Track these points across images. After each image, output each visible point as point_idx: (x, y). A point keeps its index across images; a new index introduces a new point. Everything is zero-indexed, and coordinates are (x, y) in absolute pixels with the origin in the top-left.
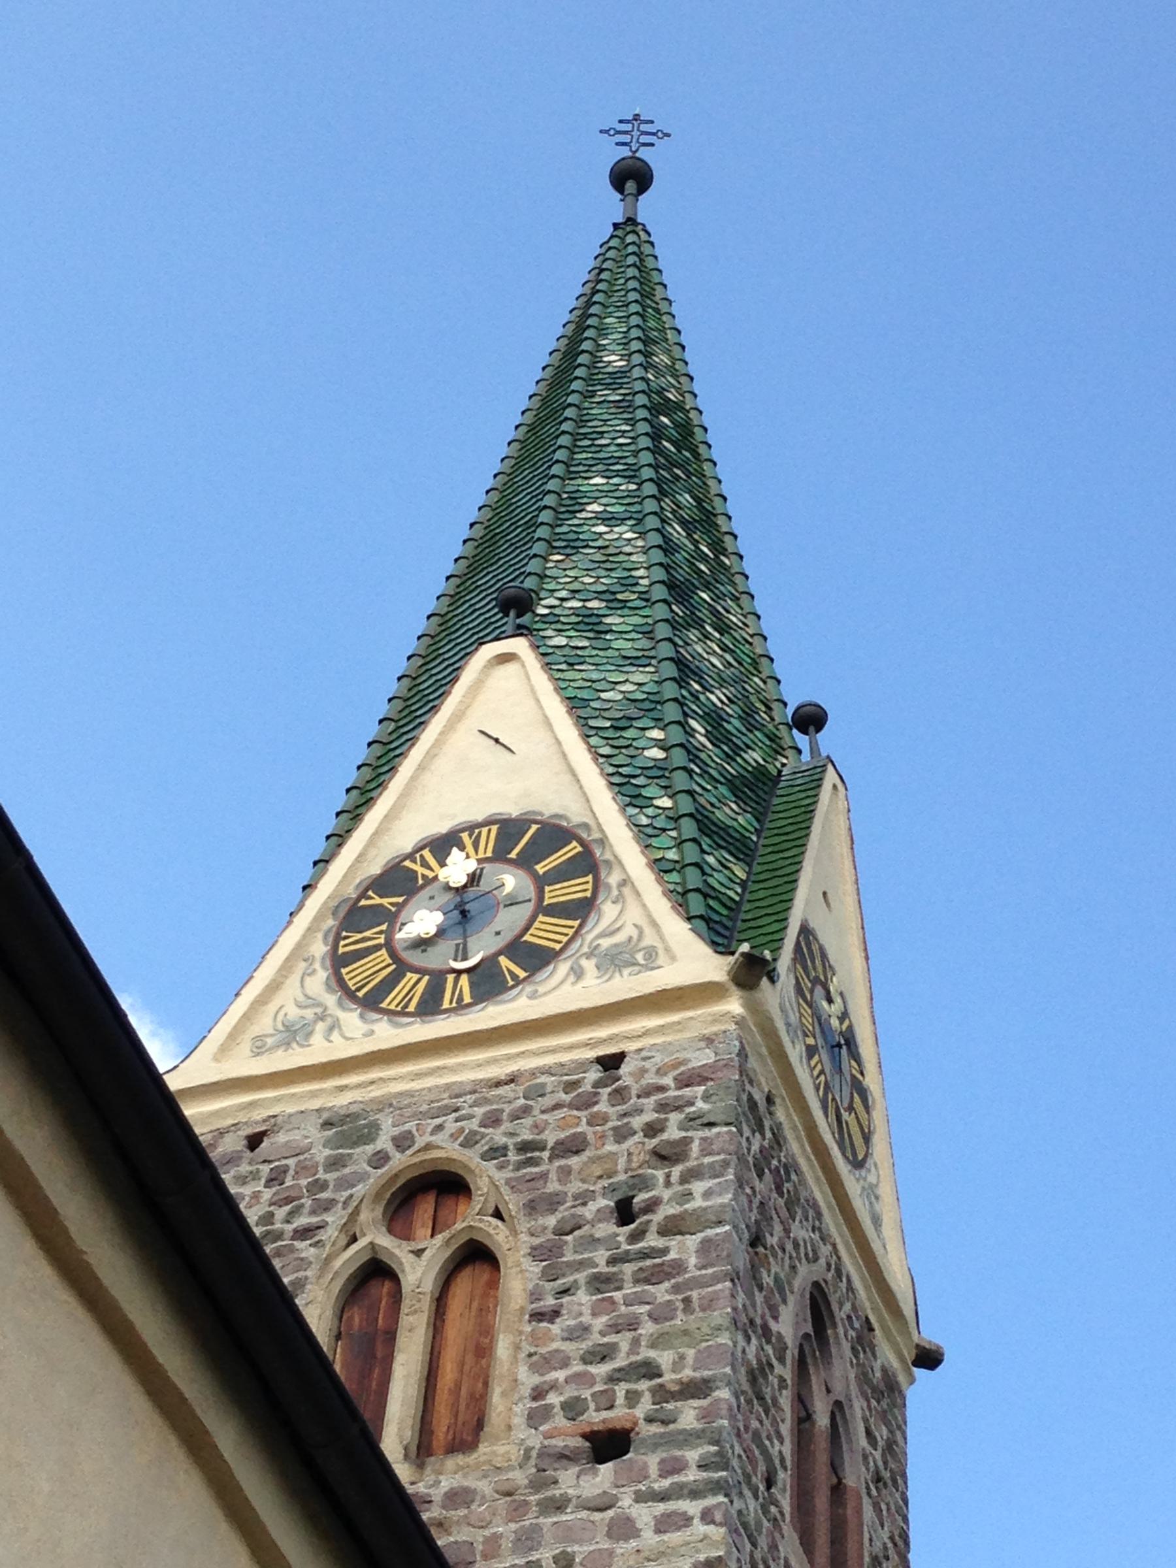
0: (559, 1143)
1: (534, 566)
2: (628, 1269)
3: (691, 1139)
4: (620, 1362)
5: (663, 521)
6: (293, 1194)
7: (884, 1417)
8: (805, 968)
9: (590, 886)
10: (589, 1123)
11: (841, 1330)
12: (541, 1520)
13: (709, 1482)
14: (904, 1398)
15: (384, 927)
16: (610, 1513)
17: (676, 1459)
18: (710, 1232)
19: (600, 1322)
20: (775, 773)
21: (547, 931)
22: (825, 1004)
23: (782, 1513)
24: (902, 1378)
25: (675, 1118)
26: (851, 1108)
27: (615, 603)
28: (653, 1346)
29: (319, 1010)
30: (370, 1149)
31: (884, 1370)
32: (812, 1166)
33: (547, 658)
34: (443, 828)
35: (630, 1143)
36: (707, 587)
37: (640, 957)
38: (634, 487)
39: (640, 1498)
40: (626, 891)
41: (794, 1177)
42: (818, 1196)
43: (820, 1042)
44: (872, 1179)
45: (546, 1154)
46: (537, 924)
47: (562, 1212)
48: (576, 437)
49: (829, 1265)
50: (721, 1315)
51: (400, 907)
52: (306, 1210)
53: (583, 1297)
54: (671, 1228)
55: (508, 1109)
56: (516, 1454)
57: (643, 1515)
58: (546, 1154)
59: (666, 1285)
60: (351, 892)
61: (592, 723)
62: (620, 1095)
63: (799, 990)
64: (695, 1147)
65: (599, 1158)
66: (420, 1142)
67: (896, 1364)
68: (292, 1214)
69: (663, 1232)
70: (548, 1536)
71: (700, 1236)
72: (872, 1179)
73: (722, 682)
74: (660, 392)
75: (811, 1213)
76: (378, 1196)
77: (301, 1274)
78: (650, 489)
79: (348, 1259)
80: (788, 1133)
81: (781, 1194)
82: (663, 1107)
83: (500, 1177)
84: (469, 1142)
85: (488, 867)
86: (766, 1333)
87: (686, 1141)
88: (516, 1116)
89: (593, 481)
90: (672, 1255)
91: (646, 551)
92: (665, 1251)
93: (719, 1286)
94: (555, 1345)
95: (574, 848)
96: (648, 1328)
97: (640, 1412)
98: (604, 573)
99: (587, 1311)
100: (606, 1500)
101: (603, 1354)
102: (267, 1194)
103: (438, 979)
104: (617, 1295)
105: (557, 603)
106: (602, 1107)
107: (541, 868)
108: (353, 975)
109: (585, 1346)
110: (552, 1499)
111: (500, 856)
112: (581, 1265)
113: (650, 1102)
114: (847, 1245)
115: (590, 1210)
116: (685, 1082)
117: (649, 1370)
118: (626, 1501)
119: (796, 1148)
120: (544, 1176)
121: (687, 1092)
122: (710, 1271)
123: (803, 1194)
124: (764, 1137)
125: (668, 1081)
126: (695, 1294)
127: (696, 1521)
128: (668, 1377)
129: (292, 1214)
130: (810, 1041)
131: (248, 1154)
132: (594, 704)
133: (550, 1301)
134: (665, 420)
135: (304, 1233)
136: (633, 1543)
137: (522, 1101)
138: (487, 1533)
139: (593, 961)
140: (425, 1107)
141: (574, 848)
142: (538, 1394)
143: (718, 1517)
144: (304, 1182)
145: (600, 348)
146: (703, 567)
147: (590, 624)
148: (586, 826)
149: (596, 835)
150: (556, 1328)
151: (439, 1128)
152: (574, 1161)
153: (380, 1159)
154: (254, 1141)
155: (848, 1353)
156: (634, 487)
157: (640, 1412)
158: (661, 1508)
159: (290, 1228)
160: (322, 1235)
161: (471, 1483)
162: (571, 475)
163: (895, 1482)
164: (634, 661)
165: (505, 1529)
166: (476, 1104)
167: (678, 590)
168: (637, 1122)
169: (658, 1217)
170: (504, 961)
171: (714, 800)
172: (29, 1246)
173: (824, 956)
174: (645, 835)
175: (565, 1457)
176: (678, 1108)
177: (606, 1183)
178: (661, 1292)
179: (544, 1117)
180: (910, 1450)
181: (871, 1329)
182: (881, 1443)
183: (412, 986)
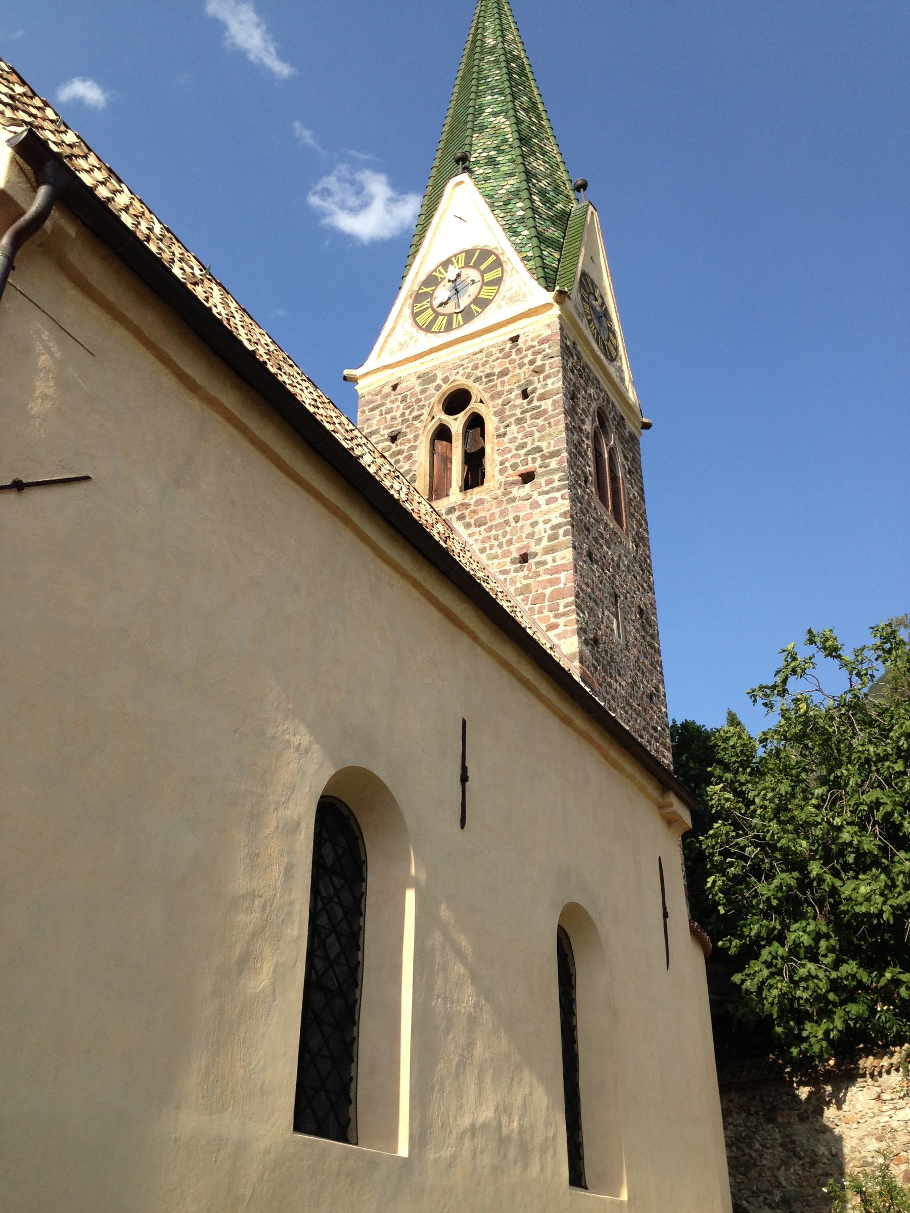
0: (500, 372)
1: (467, 141)
2: (528, 415)
3: (545, 364)
4: (529, 448)
5: (516, 111)
6: (411, 404)
7: (631, 450)
8: (585, 290)
9: (500, 272)
10: (510, 364)
11: (611, 422)
12: (508, 506)
13: (562, 485)
14: (638, 441)
15: (429, 300)
16: (530, 500)
17: (550, 479)
18: (555, 397)
19: (520, 435)
20: (569, 211)
21: (487, 293)
22: (594, 302)
23: (592, 492)
24: (637, 435)
25: (539, 357)
26: (609, 339)
27: (500, 151)
28: (539, 441)
29: (410, 335)
30: (434, 384)
31: (630, 433)
32: (594, 364)
33: (476, 181)
34: (445, 258)
35: (524, 368)
36: (536, 136)
37: (521, 298)
38: (503, 98)
39: (540, 494)
40: (514, 271)
41: (587, 370)
42: (597, 375)
43: (593, 316)
44: (619, 364)
45: (495, 377)
46: (483, 290)
47: (503, 397)
48: (478, 80)
49: (604, 400)
50: (562, 426)
51: (434, 291)
52: (416, 410)
53: (514, 428)
54: (542, 397)
55: (480, 362)
56: (497, 485)
57: (542, 500)
58: (495, 377)
59: (542, 419)
60: (416, 288)
61: (496, 204)
62: (519, 351)
63: (583, 298)
64: (547, 367)
65: (514, 376)
66: (451, 380)
67: (634, 430)
68: (411, 412)
69: (539, 399)
70: (510, 511)
71: (552, 399)
72: (619, 364)
73: (545, 177)
74: (510, 52)
75: (595, 382)
76: (439, 402)
77: (417, 433)
78: (509, 98)
79: (432, 426)
80: (583, 354)
81: (582, 378)
82: (535, 353)
83: (481, 388)
84: (468, 377)
85: (463, 270)
86: (581, 430)
87: (544, 365)
88: (483, 365)
89: (487, 99)
90: (543, 408)
91: (510, 126)
92: (540, 407)
93: (560, 416)
94: (505, 446)
95: (493, 258)
96: (537, 435)
97: (537, 464)
98: (494, 139)
99: (515, 432)
100: (529, 497)
101: (522, 446)
102: (402, 406)
103: (450, 316)
104: (525, 425)
105: (478, 155)
106: (514, 356)
107: (482, 268)
108: (421, 320)
109: (516, 444)
110: (510, 498)
111: (467, 265)
112: (512, 415)
113: (530, 352)
114: (611, 390)
115: (512, 396)
116: (541, 343)
117: (539, 449)
118: (535, 495)
119: (587, 359)
120: (496, 385)
121: (543, 346)
122: (556, 411)
123: (591, 376)
124: (573, 358)
125: (535, 343)
126: (552, 420)
127: (560, 499)
128: (545, 451)
129: (411, 412)
130: (589, 317)
131: (393, 392)
132: (496, 196)
133: (502, 430)
134: (513, 65)
135: (416, 418)
136: (539, 510)
137: (485, 359)
138: (490, 512)
139: (505, 301)
140: (451, 366)
141: (493, 258)
142: (502, 463)
143: (567, 497)
144: (413, 400)
145: (485, 37)
146: (534, 128)
147: (492, 162)
148: (496, 248)
149: (500, 251)
150: (506, 439)
151: (458, 373)
152: (506, 378)
153: (438, 388)
154: (394, 387)
155: (614, 430)
156: (503, 98)
157: (537, 464)
158: (547, 496)
159: (411, 417)
160: (422, 418)
161: (483, 496)
162: (479, 97)
163: (637, 472)
164: (511, 175)
165: (496, 511)
166: (469, 362)
167: (523, 140)
168: (526, 361)
169: (536, 394)
170: (473, 307)
171: (545, 228)
172: (274, 469)
173: (593, 282)
174: (519, 248)
175: (513, 483)
176: (540, 353)
177: (517, 384)
178: (540, 421)
179: (493, 363)
180: (642, 459)
181: (623, 419)
182: (630, 459)
183: (442, 321)
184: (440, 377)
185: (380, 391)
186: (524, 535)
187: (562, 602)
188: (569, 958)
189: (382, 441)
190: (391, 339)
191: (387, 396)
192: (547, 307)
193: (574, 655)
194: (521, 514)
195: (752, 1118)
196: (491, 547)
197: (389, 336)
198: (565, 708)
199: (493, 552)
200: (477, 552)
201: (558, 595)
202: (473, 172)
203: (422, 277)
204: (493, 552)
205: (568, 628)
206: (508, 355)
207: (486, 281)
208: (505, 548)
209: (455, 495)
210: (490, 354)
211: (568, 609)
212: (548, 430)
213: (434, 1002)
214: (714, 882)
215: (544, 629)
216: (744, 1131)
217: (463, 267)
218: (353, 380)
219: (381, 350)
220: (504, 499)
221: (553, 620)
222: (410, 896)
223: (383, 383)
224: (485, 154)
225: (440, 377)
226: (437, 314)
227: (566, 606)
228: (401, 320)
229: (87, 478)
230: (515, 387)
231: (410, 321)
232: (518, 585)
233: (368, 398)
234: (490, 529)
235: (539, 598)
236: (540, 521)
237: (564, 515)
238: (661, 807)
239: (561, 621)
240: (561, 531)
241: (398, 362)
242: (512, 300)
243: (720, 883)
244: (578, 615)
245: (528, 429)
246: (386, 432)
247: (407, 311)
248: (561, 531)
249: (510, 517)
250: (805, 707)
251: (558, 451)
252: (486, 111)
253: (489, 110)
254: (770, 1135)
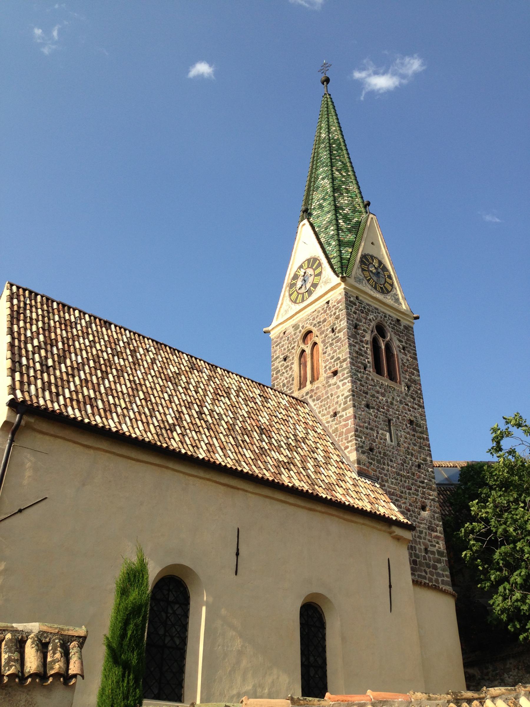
2: (334, 341)
4: (335, 358)
18: (344, 331)
19: (331, 352)
25: (337, 310)
30: (299, 330)
39: (340, 381)
55: (315, 316)
57: (340, 384)
60: (290, 281)
67: (408, 323)
76: (301, 339)
82: (336, 309)
83: (316, 329)
85: (307, 270)
87: (339, 314)
90: (340, 337)
92: (338, 336)
96: (338, 351)
102: (287, 342)
103: (303, 294)
104: (333, 346)
106: (328, 312)
107: (314, 268)
112: (328, 342)
113: (334, 309)
115: (328, 332)
116: (338, 303)
117: (339, 358)
118: (338, 382)
120: (322, 327)
125: (336, 304)
128: (341, 359)
132: (322, 226)
133: (325, 350)
135: (293, 348)
141: (318, 261)
142: (325, 367)
143: (350, 382)
147: (321, 206)
150: (326, 355)
151: (307, 323)
154: (284, 333)
157: (338, 366)
159: (291, 348)
165: (324, 392)
168: (332, 313)
175: (329, 377)
178: (339, 344)
184: (301, 326)
185: (279, 336)
186: (334, 403)
187: (350, 435)
188: (323, 615)
189: (281, 361)
190: (282, 309)
191: (282, 338)
192: (339, 284)
193: (354, 461)
194: (333, 392)
195: (520, 671)
196: (323, 410)
197: (281, 307)
198: (309, 505)
199: (323, 412)
200: (318, 413)
201: (348, 432)
202: (312, 214)
203: (292, 275)
204: (323, 412)
205: (352, 448)
206: (325, 312)
207: (296, 292)
208: (328, 410)
209: (309, 386)
210: (319, 312)
211: (352, 438)
212: (342, 348)
213: (216, 649)
214: (466, 554)
215: (343, 449)
216: (517, 678)
217: (307, 268)
218: (268, 332)
219: (278, 316)
220: (327, 386)
221: (347, 444)
222: (204, 609)
223: (280, 332)
224: (318, 203)
225: (301, 326)
226: (298, 294)
227: (351, 437)
228: (285, 298)
229: (46, 498)
230: (329, 327)
231: (288, 299)
232: (333, 428)
233: (274, 340)
234: (321, 402)
235: (341, 434)
236: (340, 395)
237: (349, 391)
238: (390, 533)
239: (350, 444)
240: (348, 399)
241: (284, 321)
242: (326, 283)
243: (468, 555)
244: (357, 440)
245: (334, 349)
246: (282, 357)
247: (287, 294)
248: (348, 399)
249: (329, 395)
250: (503, 460)
251: (346, 358)
252: (320, 177)
253: (321, 177)
254: (528, 680)
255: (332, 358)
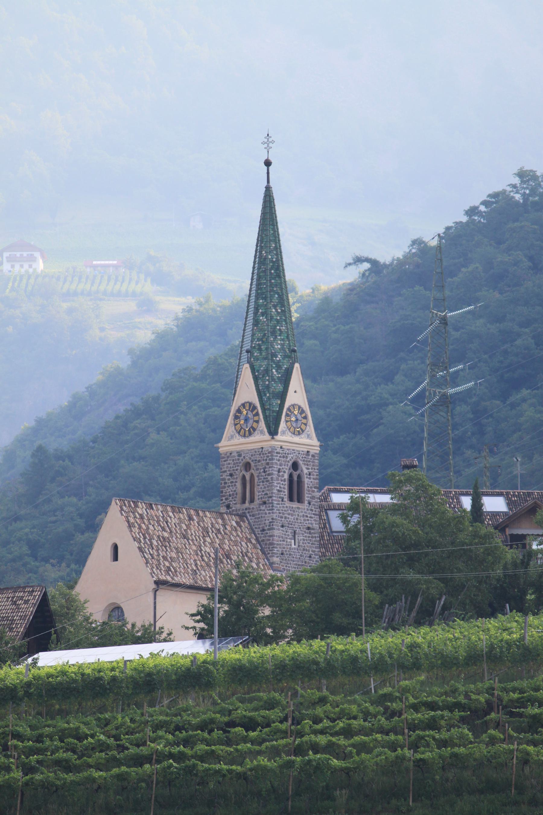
154: (231, 454)
210: (256, 452)
255: (263, 491)
